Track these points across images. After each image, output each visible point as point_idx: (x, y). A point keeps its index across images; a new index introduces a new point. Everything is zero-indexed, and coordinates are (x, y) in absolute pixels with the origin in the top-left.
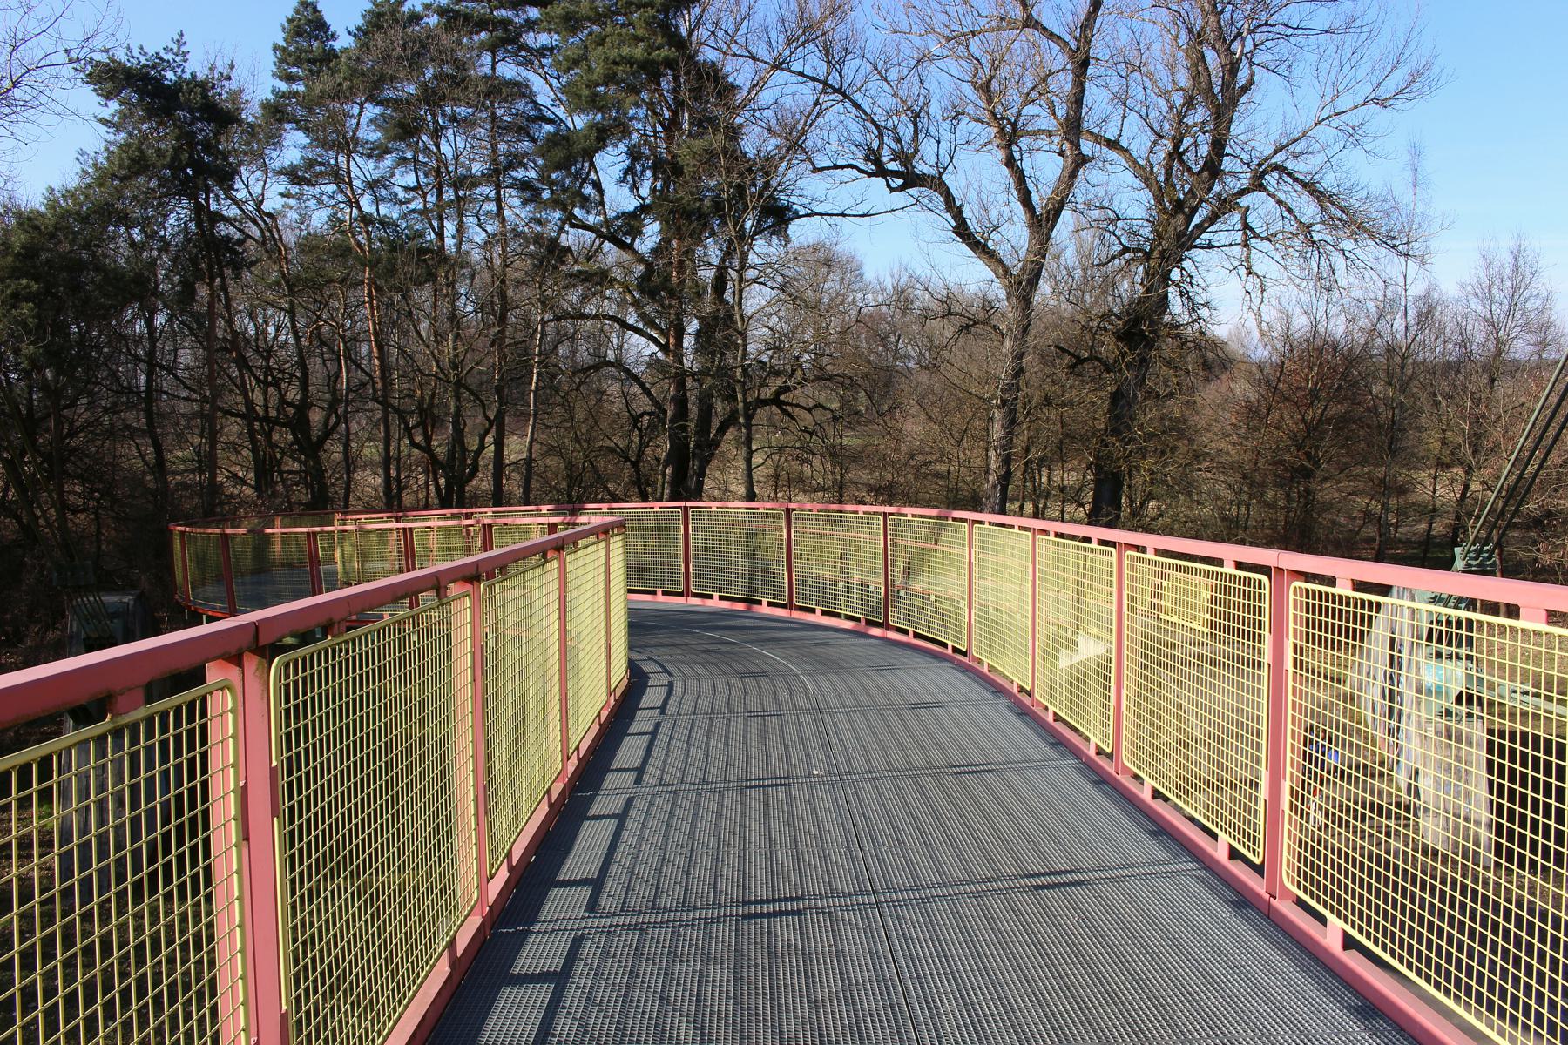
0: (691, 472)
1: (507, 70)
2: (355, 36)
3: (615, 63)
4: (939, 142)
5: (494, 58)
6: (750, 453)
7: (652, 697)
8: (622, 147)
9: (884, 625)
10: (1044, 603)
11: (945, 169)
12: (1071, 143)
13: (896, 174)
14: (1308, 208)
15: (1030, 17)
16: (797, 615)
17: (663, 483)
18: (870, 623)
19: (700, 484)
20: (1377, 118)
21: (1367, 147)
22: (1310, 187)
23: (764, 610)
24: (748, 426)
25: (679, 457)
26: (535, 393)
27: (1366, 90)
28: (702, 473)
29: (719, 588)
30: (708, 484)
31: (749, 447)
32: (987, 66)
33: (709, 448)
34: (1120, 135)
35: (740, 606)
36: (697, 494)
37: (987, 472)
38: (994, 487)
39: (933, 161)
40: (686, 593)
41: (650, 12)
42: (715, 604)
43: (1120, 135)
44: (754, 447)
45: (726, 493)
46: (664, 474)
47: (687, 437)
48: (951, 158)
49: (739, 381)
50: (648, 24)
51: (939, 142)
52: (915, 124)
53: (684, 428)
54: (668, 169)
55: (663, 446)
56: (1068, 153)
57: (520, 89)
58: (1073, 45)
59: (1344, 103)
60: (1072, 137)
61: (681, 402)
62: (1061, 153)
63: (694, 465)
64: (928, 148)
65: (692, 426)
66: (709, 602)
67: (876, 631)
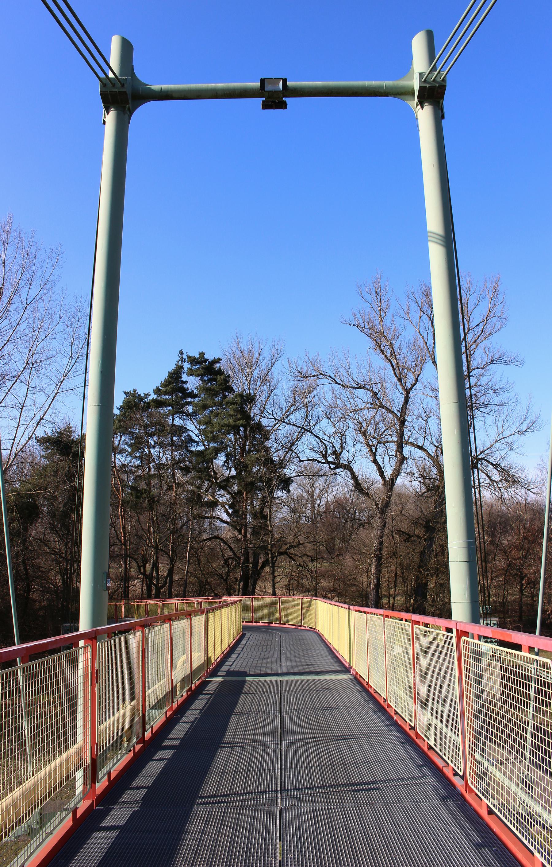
0: (250, 584)
1: (178, 421)
2: (119, 409)
3: (222, 426)
4: (348, 452)
5: (173, 418)
6: (274, 577)
7: (246, 638)
8: (224, 454)
9: (301, 626)
10: (363, 628)
11: (351, 462)
12: (399, 452)
13: (332, 463)
14: (496, 476)
15: (381, 404)
16: (281, 626)
17: (239, 589)
18: (299, 626)
19: (254, 589)
20: (519, 440)
21: (516, 451)
22: (496, 466)
23: (273, 625)
24: (273, 567)
25: (245, 578)
26: (189, 553)
27: (514, 429)
28: (255, 584)
29: (261, 619)
30: (257, 589)
31: (274, 575)
32: (365, 426)
33: (257, 573)
34: (423, 444)
35: (266, 624)
36: (253, 593)
37: (370, 584)
38: (373, 589)
39: (346, 459)
40: (252, 622)
41: (235, 406)
42: (261, 624)
43: (423, 444)
44: (276, 575)
45: (265, 593)
46: (239, 585)
47: (249, 570)
48: (354, 458)
49: (269, 550)
50: (235, 410)
51: (348, 452)
52: (341, 440)
53: (247, 567)
54: (241, 467)
55: (239, 574)
56: (398, 456)
57: (183, 429)
58: (399, 415)
59: (506, 434)
60: (399, 450)
61: (246, 554)
62: (396, 456)
63: (251, 582)
64: (344, 455)
65: (251, 565)
66: (258, 624)
67: (299, 628)
